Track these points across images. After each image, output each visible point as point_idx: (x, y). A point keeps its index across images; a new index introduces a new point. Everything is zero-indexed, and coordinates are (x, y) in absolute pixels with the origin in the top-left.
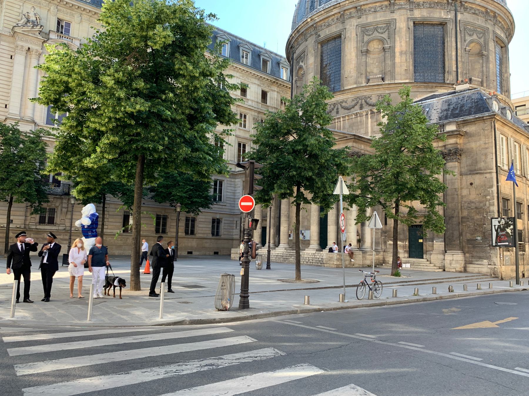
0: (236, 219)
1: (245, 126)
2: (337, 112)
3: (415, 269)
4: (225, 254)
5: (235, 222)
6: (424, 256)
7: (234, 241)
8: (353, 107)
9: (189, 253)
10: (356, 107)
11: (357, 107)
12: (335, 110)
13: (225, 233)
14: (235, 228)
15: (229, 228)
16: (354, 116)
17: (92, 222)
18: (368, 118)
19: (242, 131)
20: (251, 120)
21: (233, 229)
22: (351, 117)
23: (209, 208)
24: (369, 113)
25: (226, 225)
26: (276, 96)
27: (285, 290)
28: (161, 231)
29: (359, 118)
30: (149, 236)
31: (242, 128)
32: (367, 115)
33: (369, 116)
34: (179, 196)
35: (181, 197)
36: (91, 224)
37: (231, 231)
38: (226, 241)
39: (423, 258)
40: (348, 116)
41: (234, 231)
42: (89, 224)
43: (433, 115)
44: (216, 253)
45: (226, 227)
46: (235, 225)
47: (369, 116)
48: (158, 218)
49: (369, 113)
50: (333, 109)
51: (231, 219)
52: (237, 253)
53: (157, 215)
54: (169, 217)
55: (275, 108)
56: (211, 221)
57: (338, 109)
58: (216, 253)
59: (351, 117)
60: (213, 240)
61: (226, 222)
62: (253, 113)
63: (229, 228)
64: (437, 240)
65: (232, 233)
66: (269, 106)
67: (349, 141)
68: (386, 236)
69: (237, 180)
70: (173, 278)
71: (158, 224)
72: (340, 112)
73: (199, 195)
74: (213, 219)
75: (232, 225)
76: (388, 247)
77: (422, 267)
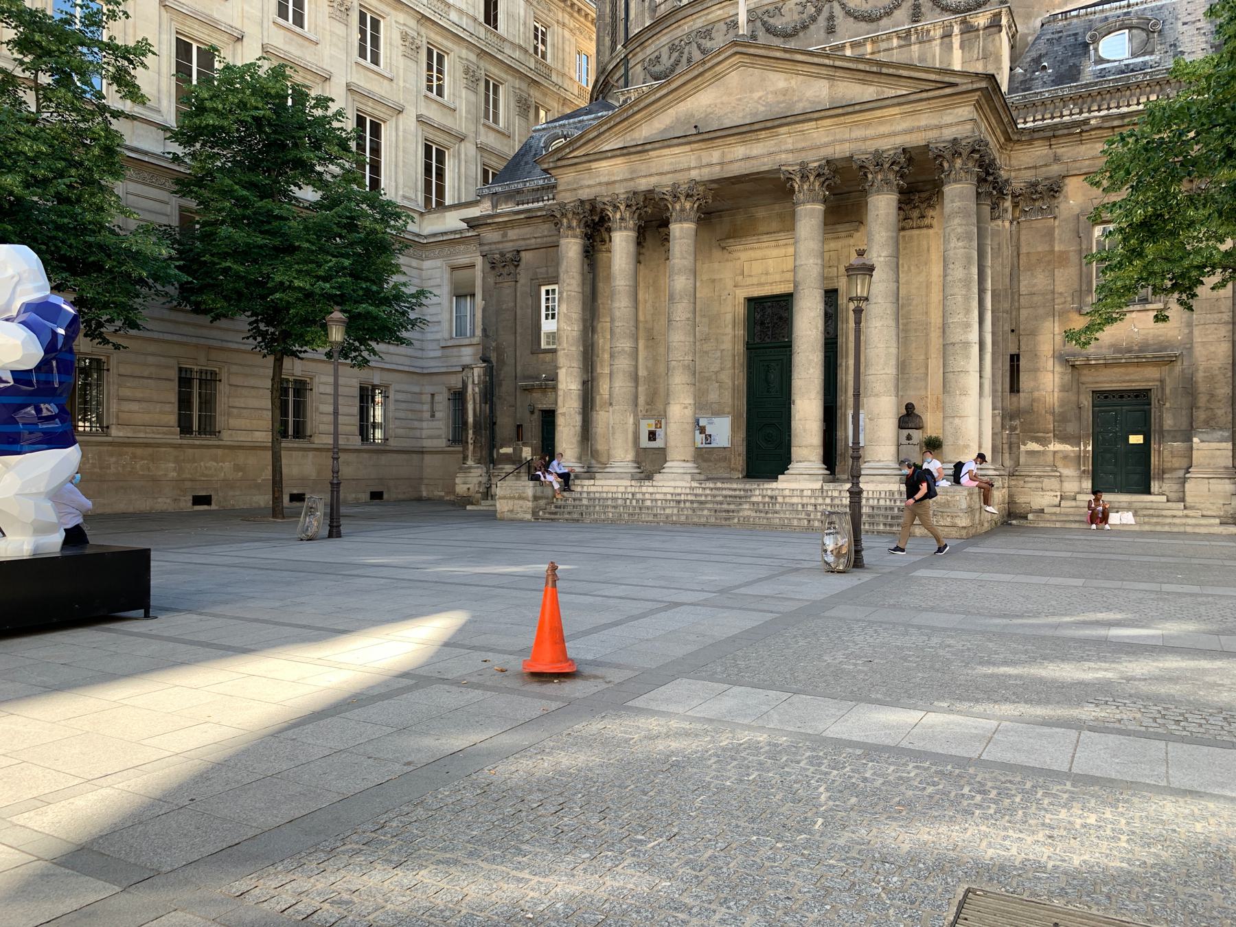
0: (429, 389)
1: (440, 93)
2: (831, 30)
3: (1158, 528)
4: (401, 496)
5: (427, 398)
6: (1155, 486)
7: (427, 458)
8: (888, 13)
9: (198, 500)
10: (897, 13)
11: (902, 14)
12: (822, 21)
13: (400, 432)
14: (427, 415)
15: (410, 415)
16: (895, 42)
17: (50, 348)
18: (950, 48)
19: (434, 106)
20: (460, 74)
21: (421, 420)
22: (884, 45)
23: (401, 341)
24: (956, 30)
25: (404, 406)
26: (522, 13)
27: (692, 604)
28: (195, 427)
29: (915, 48)
30: (159, 445)
31: (434, 95)
32: (947, 35)
33: (956, 41)
34: (300, 289)
35: (309, 295)
36: (43, 365)
37: (416, 424)
38: (405, 456)
39: (1149, 493)
40: (874, 41)
41: (425, 425)
42: (31, 365)
43: (1184, 39)
44: (376, 496)
45: (401, 415)
46: (426, 407)
47: (956, 41)
48: (185, 381)
49: (956, 30)
50: (814, 19)
51: (416, 389)
52: (520, 498)
53: (180, 369)
54: (224, 376)
55: (520, 47)
56: (356, 392)
57: (831, 18)
58: (376, 496)
59: (884, 45)
60: (366, 455)
61: (400, 397)
62: (464, 53)
63: (410, 415)
64: (1205, 437)
65: (418, 433)
66: (504, 40)
67: (957, 99)
68: (1013, 429)
69: (427, 264)
70: (534, 614)
71: (184, 402)
72: (838, 29)
73: (367, 290)
74: (362, 389)
75: (418, 407)
76: (1022, 460)
77: (1169, 520)
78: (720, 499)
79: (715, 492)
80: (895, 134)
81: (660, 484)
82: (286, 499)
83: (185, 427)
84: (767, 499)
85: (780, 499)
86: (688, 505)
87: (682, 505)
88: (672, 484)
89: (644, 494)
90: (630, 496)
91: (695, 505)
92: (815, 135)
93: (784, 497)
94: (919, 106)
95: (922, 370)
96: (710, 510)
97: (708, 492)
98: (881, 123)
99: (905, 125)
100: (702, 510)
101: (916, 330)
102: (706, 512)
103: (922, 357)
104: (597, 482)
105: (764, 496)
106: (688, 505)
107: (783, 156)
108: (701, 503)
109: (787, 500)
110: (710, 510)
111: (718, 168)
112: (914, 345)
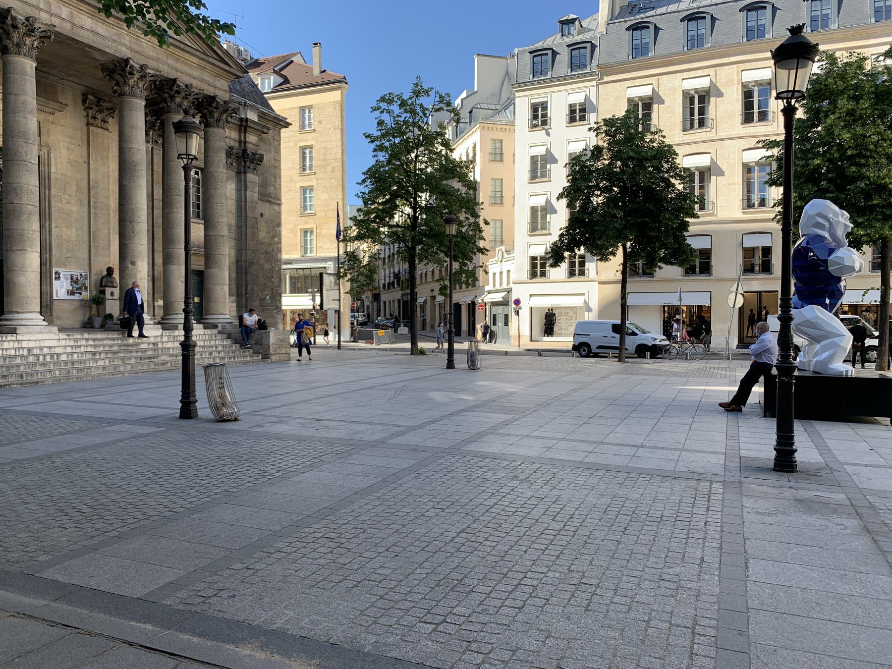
78: (115, 348)
79: (97, 343)
80: (191, 76)
81: (26, 337)
82: (549, 342)
83: (534, 275)
84: (151, 346)
85: (160, 345)
86: (103, 355)
87: (98, 356)
88: (39, 337)
89: (41, 348)
90: (25, 352)
91: (109, 355)
92: (145, 45)
93: (162, 343)
94: (208, 66)
95: (106, 242)
96: (136, 358)
97: (91, 343)
98: (185, 64)
99: (196, 73)
100: (130, 358)
101: (102, 209)
102: (133, 361)
103: (106, 231)
104: (19, 337)
105: (149, 344)
106: (103, 355)
107: (123, 49)
108: (114, 353)
109: (165, 345)
110: (136, 358)
111: (68, 25)
112: (101, 221)
